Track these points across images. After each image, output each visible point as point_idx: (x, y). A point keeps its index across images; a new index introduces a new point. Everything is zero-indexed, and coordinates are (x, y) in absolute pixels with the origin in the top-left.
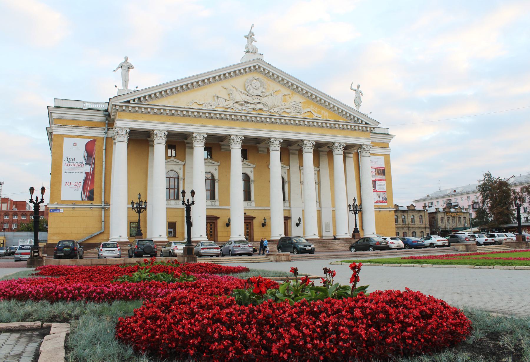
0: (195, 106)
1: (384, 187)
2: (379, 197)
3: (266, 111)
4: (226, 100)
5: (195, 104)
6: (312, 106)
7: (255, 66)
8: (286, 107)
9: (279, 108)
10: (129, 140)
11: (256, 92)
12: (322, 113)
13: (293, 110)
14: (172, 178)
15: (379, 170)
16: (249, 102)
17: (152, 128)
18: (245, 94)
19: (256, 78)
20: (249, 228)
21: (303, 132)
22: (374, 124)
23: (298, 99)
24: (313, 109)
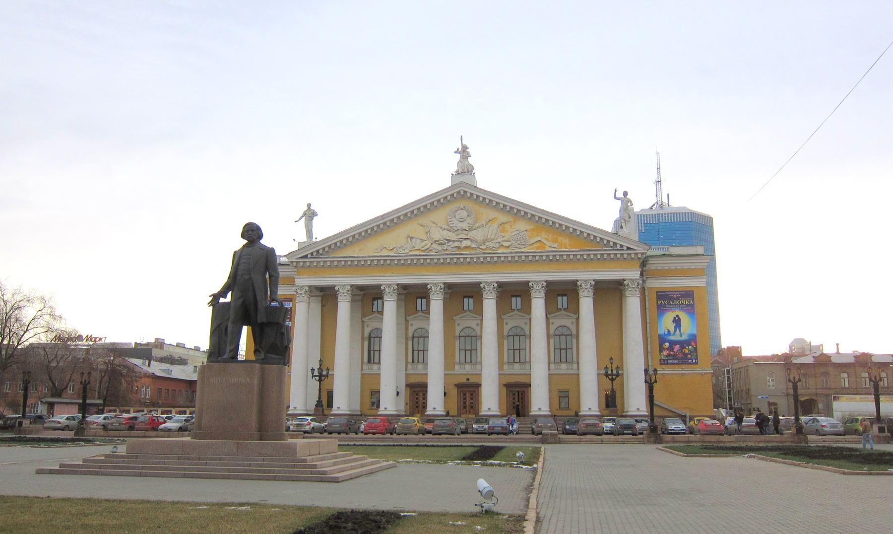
0: (385, 253)
3: (475, 248)
4: (422, 240)
5: (385, 250)
6: (544, 233)
7: (459, 192)
8: (503, 239)
9: (494, 241)
10: (352, 300)
11: (460, 225)
13: (513, 242)
14: (468, 336)
16: (451, 239)
17: (622, 278)
18: (447, 230)
19: (462, 206)
20: (474, 399)
21: (286, 273)
22: (642, 248)
23: (522, 226)
24: (546, 236)
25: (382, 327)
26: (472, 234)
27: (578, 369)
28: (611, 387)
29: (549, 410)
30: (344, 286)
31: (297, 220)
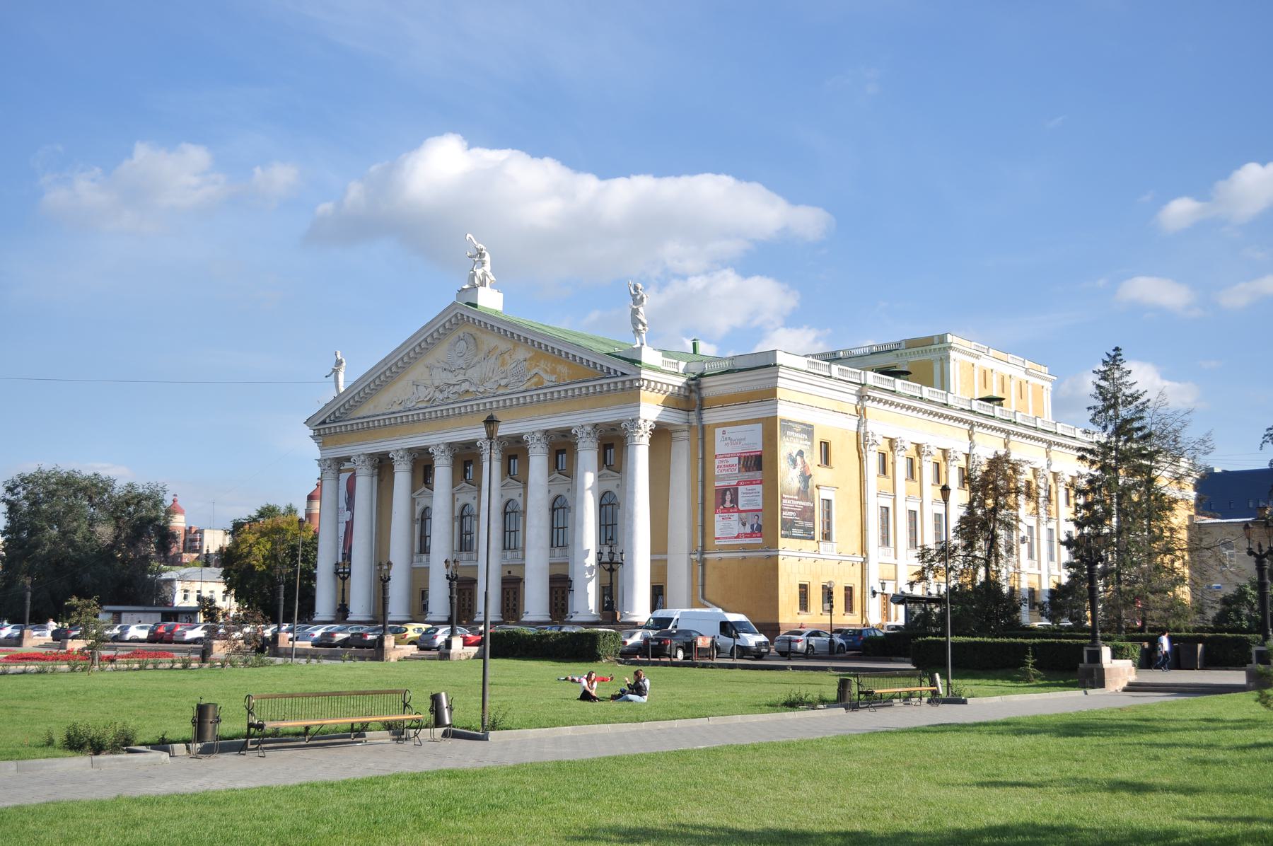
1: (757, 498)
2: (744, 524)
12: (558, 370)
15: (747, 458)
25: (432, 505)
26: (470, 373)
27: (523, 559)
28: (609, 581)
29: (501, 615)
30: (359, 456)
31: (328, 374)
